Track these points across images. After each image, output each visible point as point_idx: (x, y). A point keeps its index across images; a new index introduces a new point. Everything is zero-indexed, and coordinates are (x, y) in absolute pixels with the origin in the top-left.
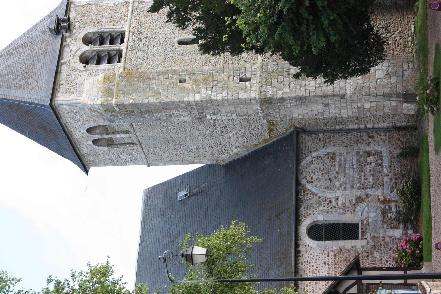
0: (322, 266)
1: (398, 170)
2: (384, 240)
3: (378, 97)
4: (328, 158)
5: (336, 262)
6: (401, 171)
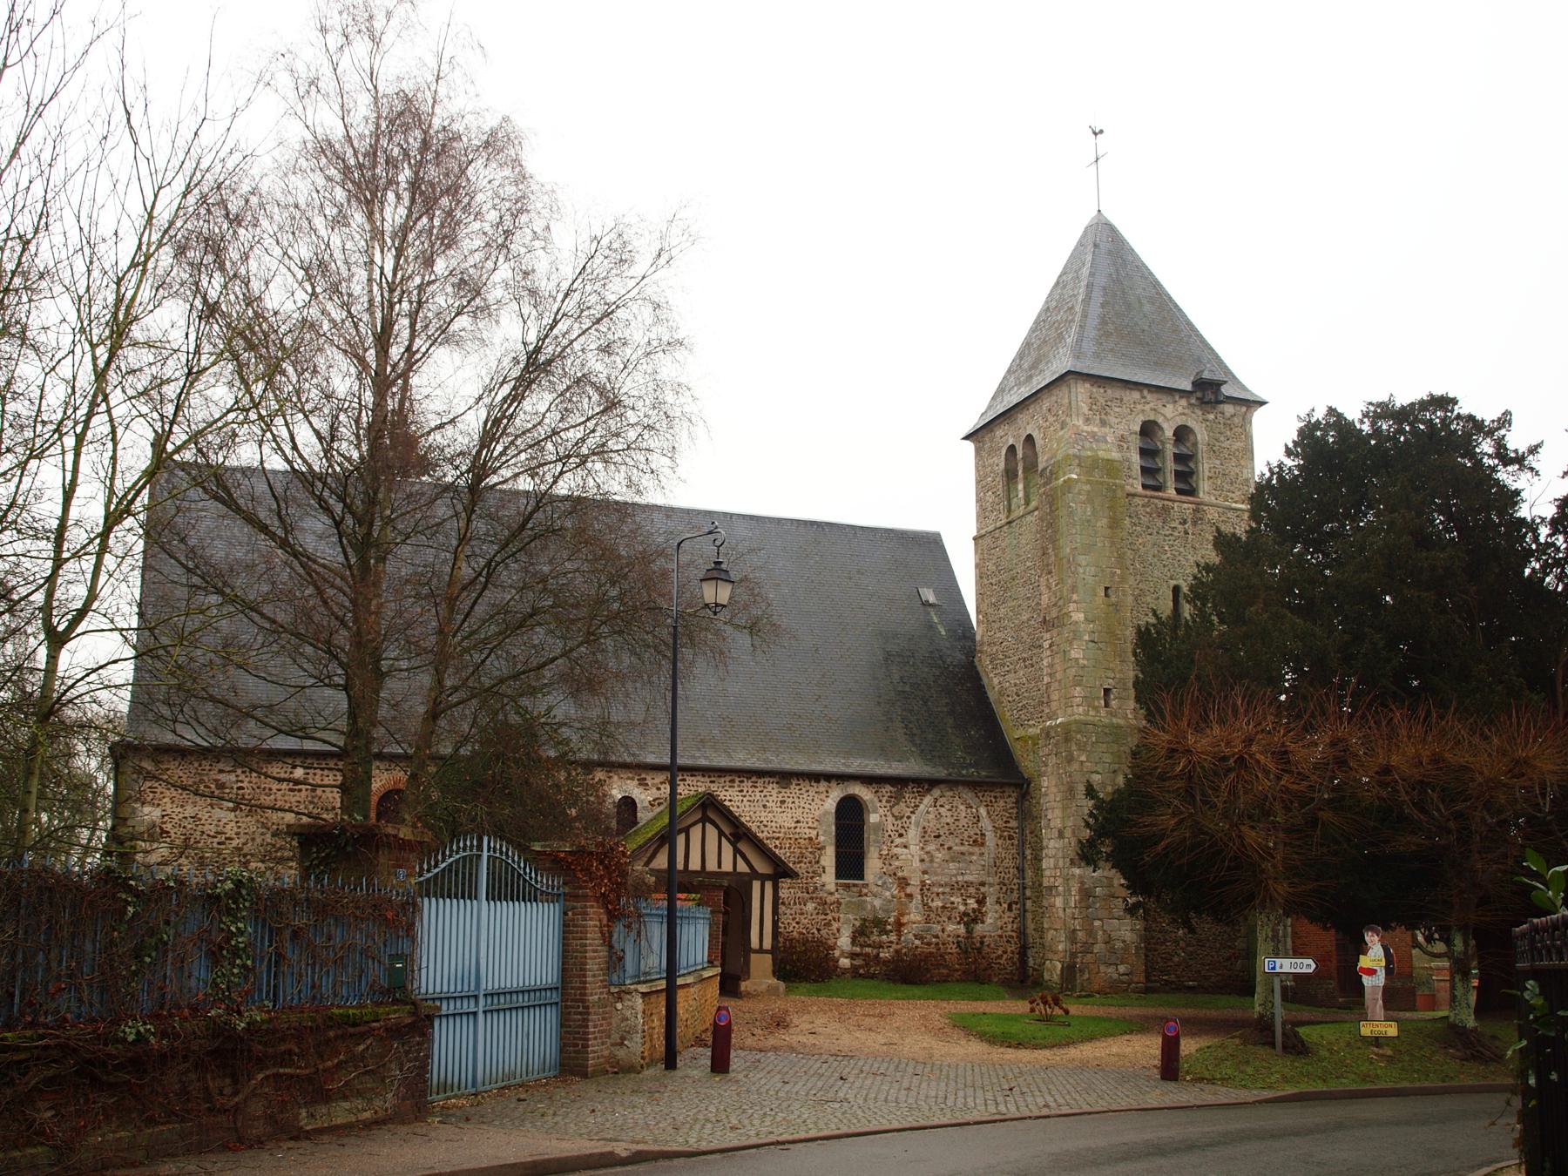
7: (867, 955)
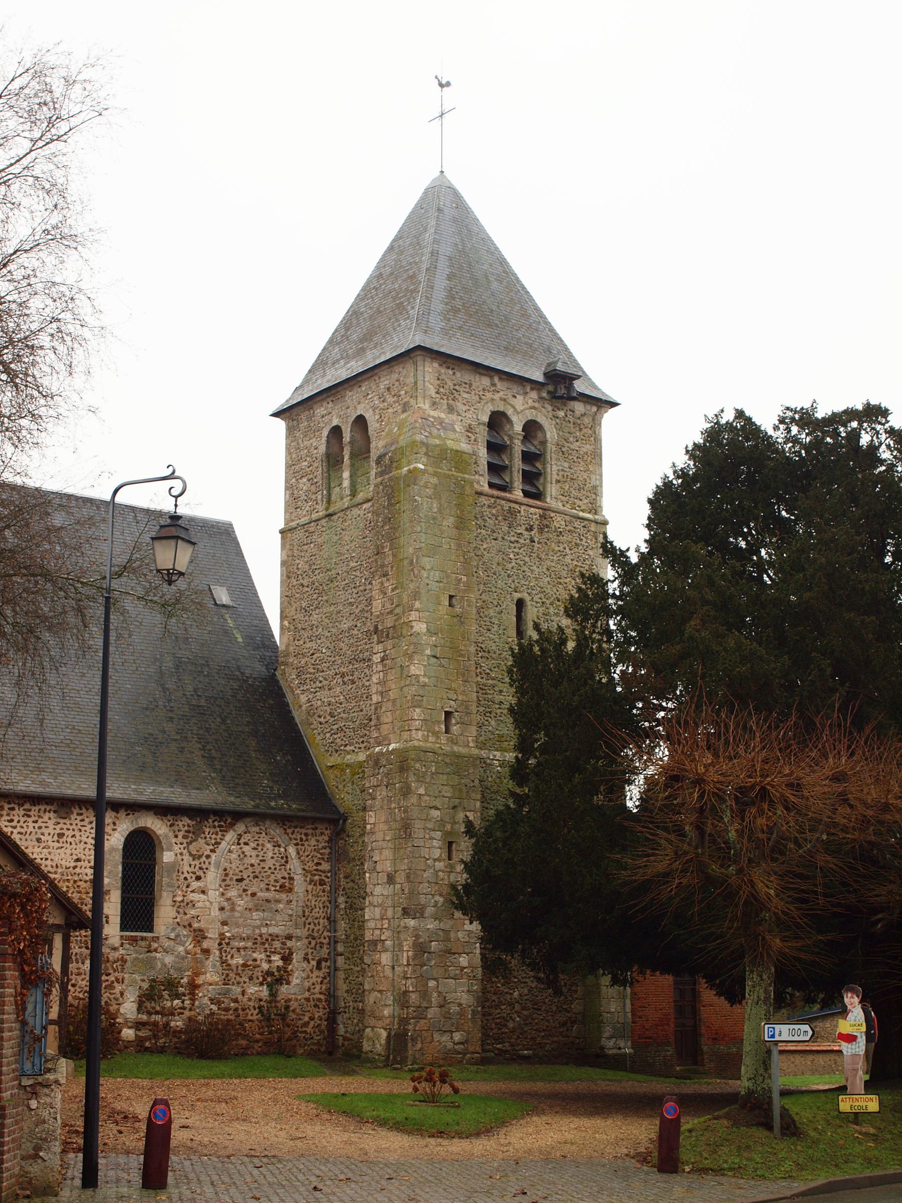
0: (72, 855)
1: (252, 1015)
2: (117, 980)
3: (404, 982)
4: (284, 878)
5: (79, 883)
6: (250, 1021)
7: (155, 1024)
